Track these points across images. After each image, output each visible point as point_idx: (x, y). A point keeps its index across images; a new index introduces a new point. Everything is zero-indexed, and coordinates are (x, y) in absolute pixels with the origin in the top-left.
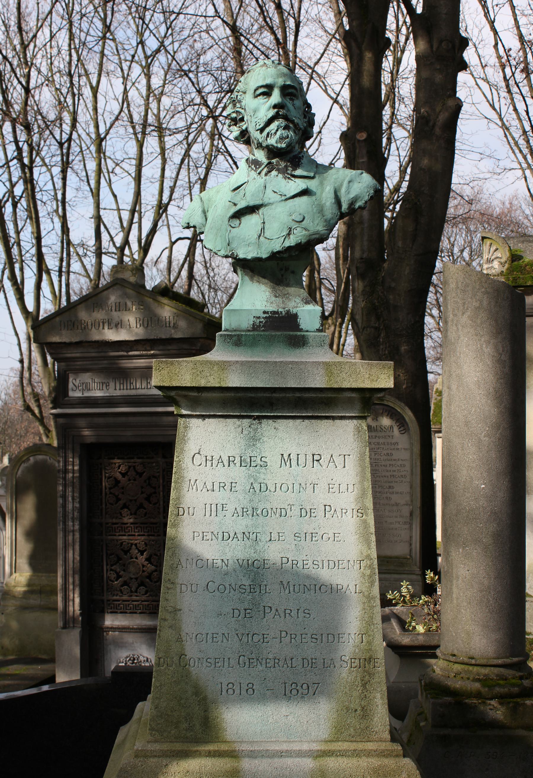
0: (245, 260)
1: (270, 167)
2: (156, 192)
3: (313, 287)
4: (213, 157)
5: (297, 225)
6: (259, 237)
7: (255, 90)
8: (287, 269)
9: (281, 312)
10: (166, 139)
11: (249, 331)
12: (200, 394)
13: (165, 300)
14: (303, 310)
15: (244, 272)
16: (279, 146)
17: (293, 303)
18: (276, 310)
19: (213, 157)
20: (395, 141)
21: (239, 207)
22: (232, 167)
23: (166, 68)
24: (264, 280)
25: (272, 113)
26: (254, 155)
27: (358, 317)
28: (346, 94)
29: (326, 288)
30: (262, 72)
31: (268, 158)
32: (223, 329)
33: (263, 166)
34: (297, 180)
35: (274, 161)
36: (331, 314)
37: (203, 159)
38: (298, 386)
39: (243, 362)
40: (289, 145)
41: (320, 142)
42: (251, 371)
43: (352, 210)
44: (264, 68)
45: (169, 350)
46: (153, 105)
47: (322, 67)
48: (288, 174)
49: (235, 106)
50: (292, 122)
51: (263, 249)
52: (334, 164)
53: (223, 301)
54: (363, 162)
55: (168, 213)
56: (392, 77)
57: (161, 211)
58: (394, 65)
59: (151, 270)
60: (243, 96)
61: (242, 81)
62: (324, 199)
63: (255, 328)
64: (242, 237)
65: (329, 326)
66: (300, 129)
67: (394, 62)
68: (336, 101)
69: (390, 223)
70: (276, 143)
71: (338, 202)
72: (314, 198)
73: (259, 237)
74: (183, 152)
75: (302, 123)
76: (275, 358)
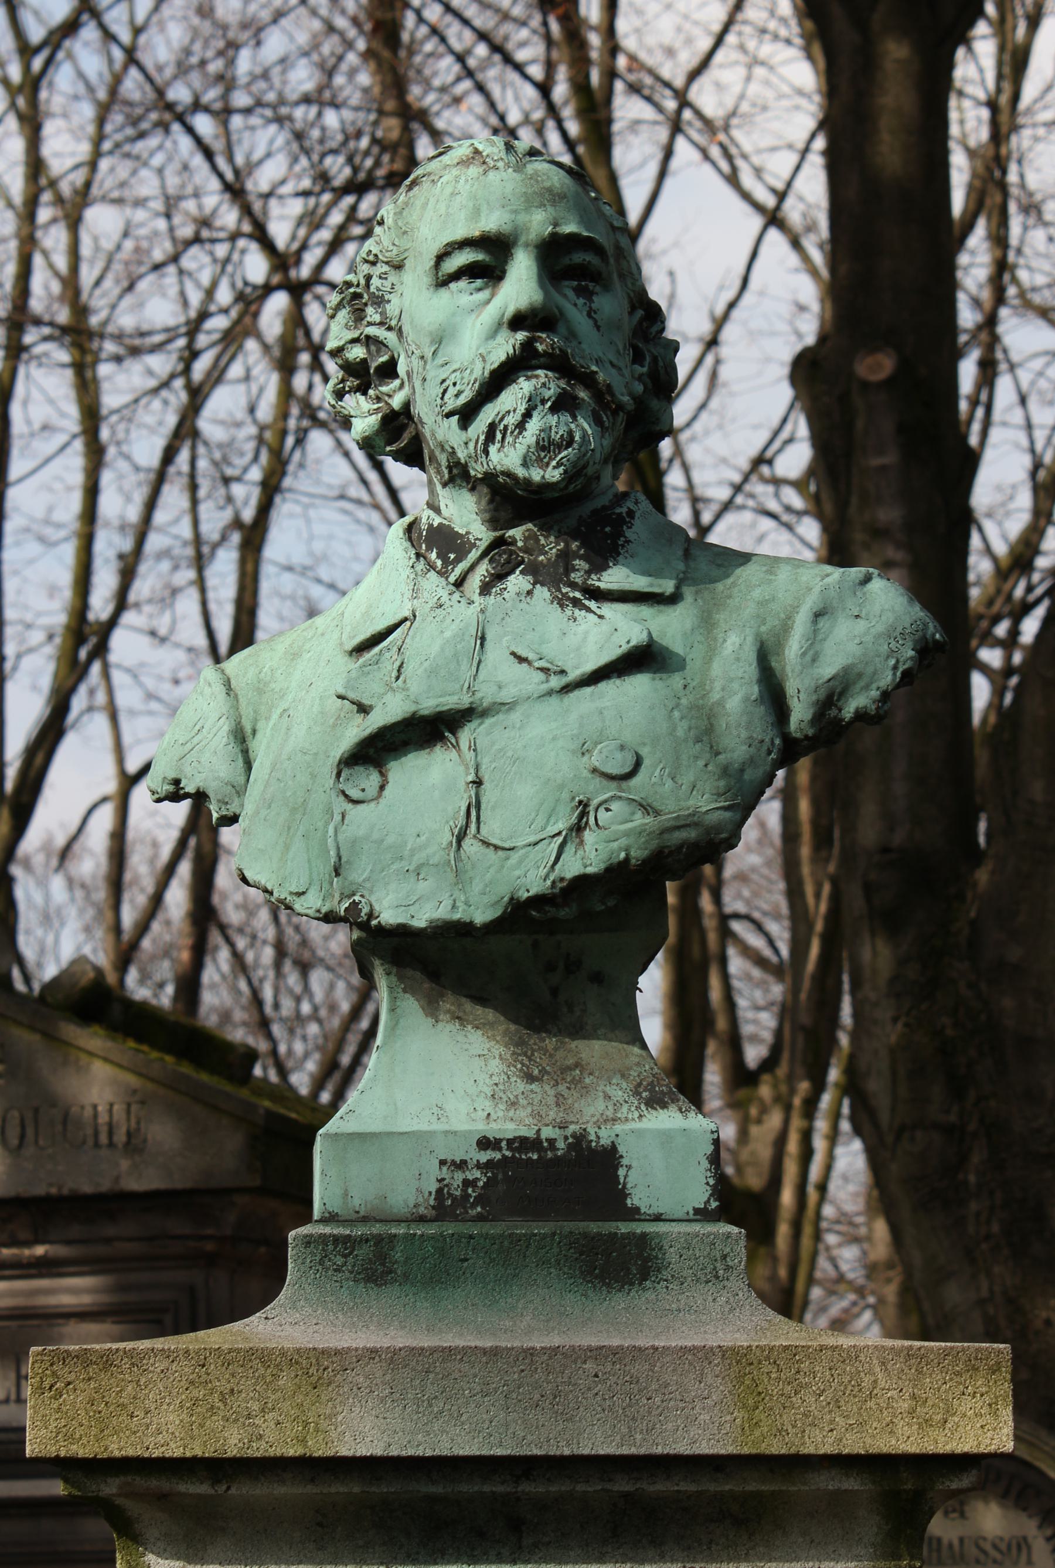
0: (403, 931)
1: (503, 560)
2: (65, 577)
3: (696, 951)
4: (290, 441)
5: (610, 790)
6: (460, 838)
7: (440, 258)
8: (572, 966)
9: (552, 1142)
10: (104, 369)
11: (422, 1219)
12: (221, 1488)
13: (91, 1039)
14: (638, 1133)
15: (401, 978)
16: (536, 475)
17: (600, 1105)
18: (531, 1134)
19: (290, 441)
20: (1012, 367)
21: (377, 720)
22: (364, 482)
23: (102, 95)
24: (479, 1010)
25: (505, 347)
26: (437, 510)
27: (876, 1086)
28: (812, 190)
29: (747, 951)
30: (467, 185)
31: (494, 523)
32: (316, 1214)
33: (474, 555)
34: (608, 610)
35: (516, 533)
36: (769, 1064)
37: (250, 447)
38: (625, 1451)
39: (396, 1351)
40: (574, 473)
41: (714, 376)
42: (431, 1390)
43: (831, 732)
44: (474, 171)
45: (108, 1241)
46: (54, 239)
47: (719, 86)
48: (573, 585)
49: (359, 315)
50: (588, 380)
51: (477, 887)
52: (770, 462)
53: (333, 1008)
54: (883, 468)
55: (113, 657)
56: (994, 123)
57: (83, 654)
58: (1000, 77)
59: (43, 883)
60: (393, 278)
61: (389, 221)
62: (718, 685)
63: (445, 1206)
64: (390, 840)
65: (764, 1110)
66: (620, 407)
67: (1000, 64)
68: (774, 219)
69: (998, 692)
70: (525, 464)
71: (773, 694)
72: (676, 680)
73: (460, 838)
74: (172, 420)
75: (622, 382)
76: (529, 1331)
